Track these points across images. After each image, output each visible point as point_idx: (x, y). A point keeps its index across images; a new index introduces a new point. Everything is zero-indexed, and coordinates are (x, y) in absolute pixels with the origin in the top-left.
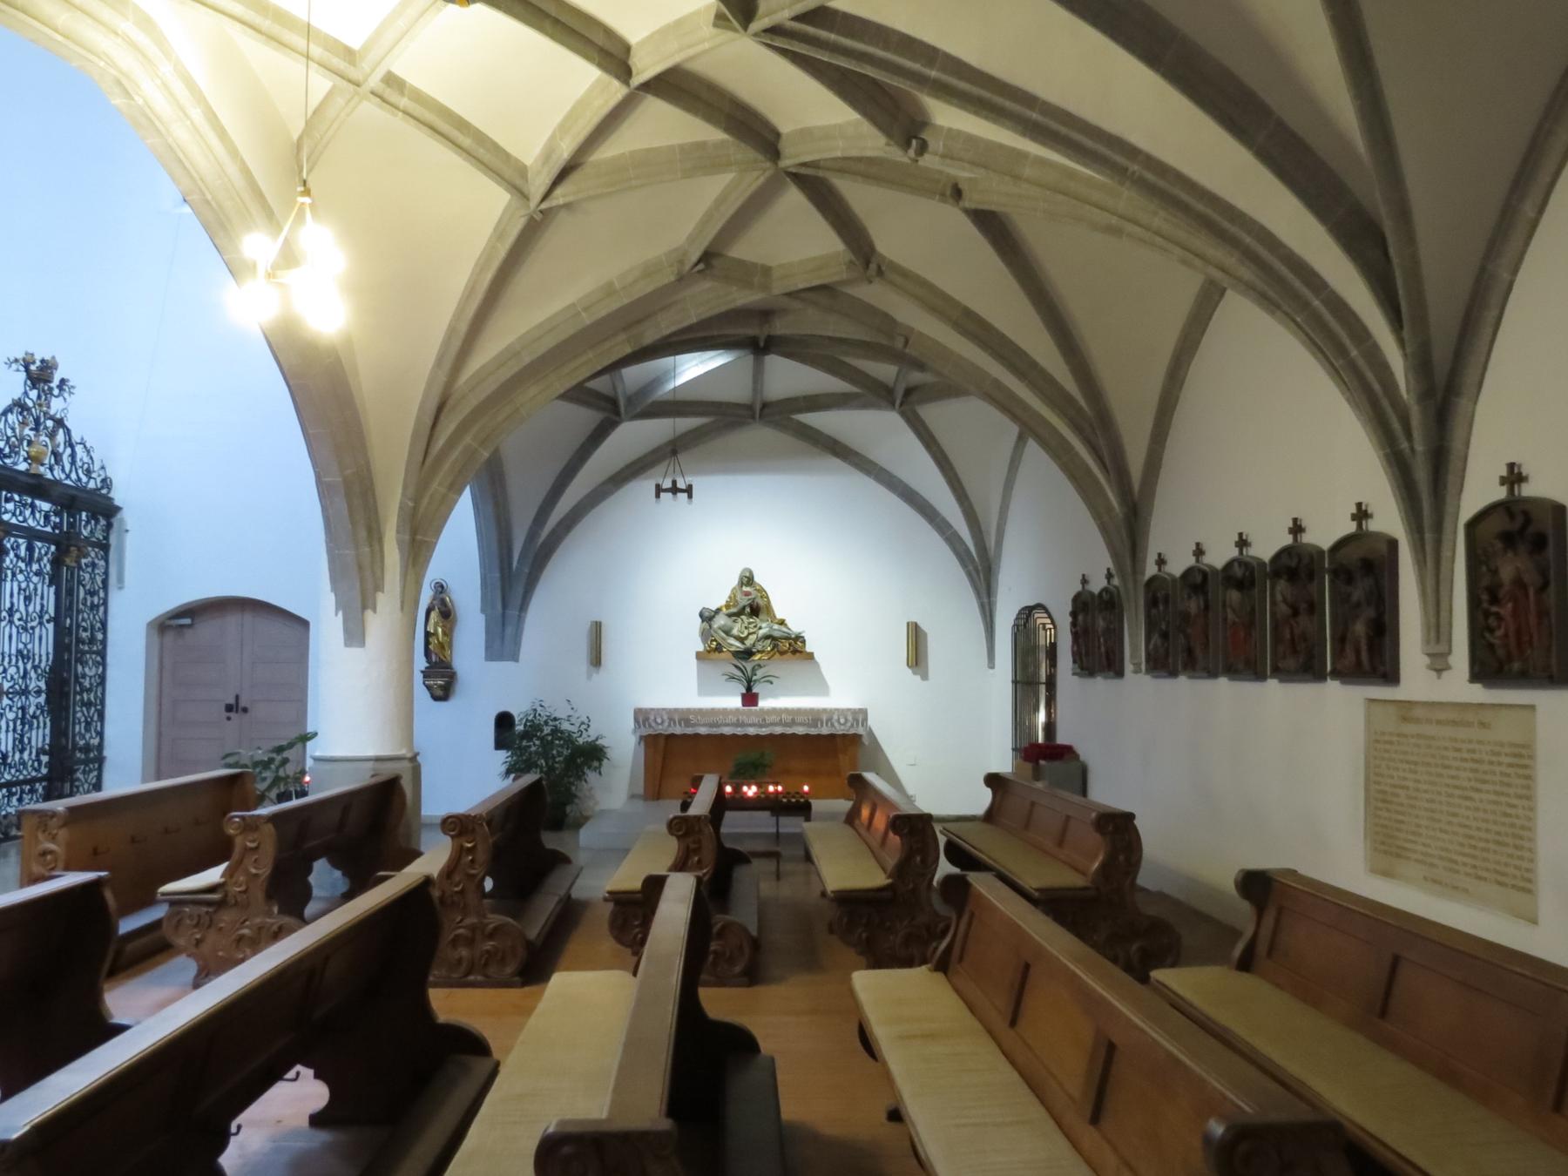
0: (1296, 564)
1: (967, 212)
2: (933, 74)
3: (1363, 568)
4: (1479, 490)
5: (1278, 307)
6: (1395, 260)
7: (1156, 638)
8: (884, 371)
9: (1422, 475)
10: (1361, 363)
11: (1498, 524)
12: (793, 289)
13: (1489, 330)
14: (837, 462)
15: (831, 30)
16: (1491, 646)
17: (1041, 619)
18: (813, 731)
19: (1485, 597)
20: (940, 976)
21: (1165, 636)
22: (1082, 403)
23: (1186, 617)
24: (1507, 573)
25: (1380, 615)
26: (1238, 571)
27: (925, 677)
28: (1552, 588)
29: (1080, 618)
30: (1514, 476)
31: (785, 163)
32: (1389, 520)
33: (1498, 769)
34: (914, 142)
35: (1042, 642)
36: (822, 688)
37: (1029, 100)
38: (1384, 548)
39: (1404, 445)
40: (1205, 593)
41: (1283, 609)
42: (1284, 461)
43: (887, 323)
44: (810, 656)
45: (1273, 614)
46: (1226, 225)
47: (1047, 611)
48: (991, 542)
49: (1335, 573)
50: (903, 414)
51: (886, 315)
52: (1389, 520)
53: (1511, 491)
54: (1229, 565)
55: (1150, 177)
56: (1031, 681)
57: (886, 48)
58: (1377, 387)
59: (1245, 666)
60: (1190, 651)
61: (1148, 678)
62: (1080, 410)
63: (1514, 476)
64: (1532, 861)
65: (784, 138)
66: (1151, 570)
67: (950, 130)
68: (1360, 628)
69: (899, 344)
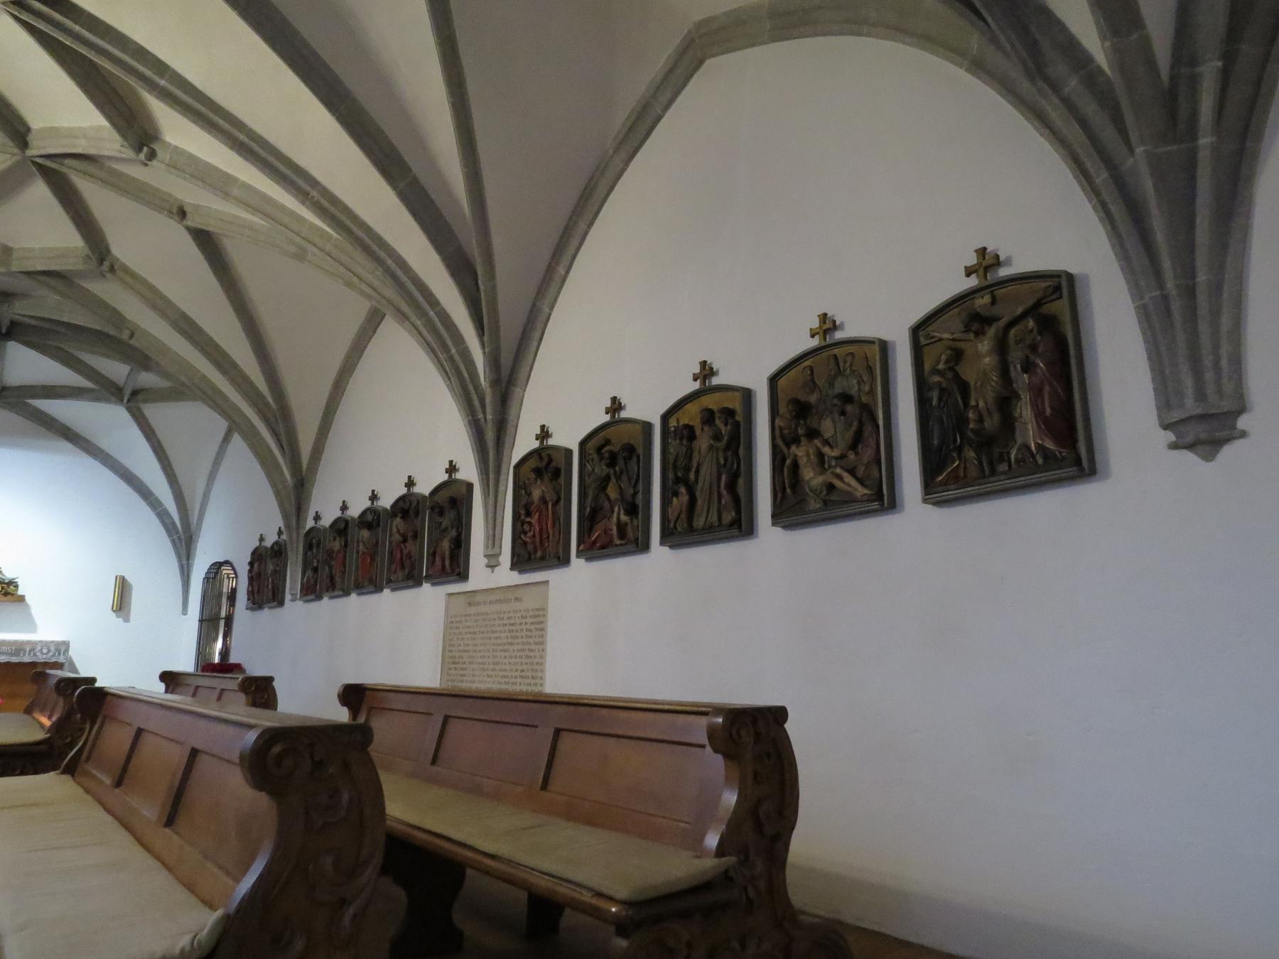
0: (407, 506)
1: (188, 229)
2: (163, 83)
3: (451, 502)
4: (524, 443)
5: (408, 319)
6: (482, 287)
7: (309, 573)
8: (117, 370)
9: (490, 435)
10: (457, 358)
11: (532, 463)
12: (31, 269)
13: (535, 344)
14: (69, 445)
15: (76, 23)
16: (525, 543)
17: (226, 570)
18: (15, 659)
19: (523, 512)
20: (67, 778)
21: (315, 570)
22: (270, 399)
23: (330, 553)
24: (536, 494)
25: (459, 535)
26: (369, 517)
27: (127, 620)
28: (562, 503)
29: (256, 565)
30: (544, 434)
31: (31, 152)
32: (469, 471)
33: (524, 627)
34: (145, 149)
35: (225, 590)
36: (32, 627)
37: (240, 125)
38: (464, 490)
39: (481, 416)
40: (346, 535)
41: (397, 537)
42: (404, 437)
43: (117, 318)
44: (21, 599)
45: (390, 543)
46: (375, 248)
47: (232, 565)
48: (194, 519)
49: (432, 509)
50: (129, 409)
51: (114, 309)
52: (469, 471)
53: (542, 443)
54: (364, 513)
55: (326, 204)
56: (214, 620)
57: (123, 51)
58: (466, 374)
59: (370, 583)
60: (332, 578)
61: (301, 603)
62: (267, 404)
63: (544, 434)
64: (542, 657)
65: (33, 132)
66: (310, 523)
67: (176, 147)
68: (446, 545)
69: (125, 335)
